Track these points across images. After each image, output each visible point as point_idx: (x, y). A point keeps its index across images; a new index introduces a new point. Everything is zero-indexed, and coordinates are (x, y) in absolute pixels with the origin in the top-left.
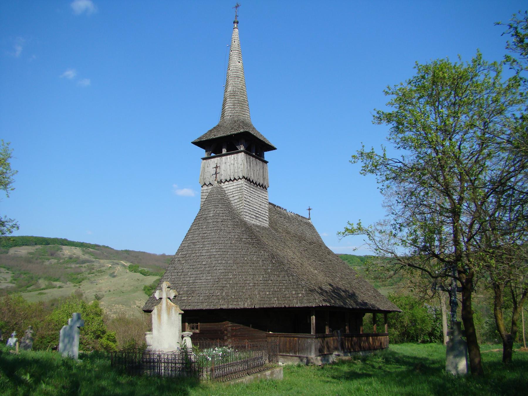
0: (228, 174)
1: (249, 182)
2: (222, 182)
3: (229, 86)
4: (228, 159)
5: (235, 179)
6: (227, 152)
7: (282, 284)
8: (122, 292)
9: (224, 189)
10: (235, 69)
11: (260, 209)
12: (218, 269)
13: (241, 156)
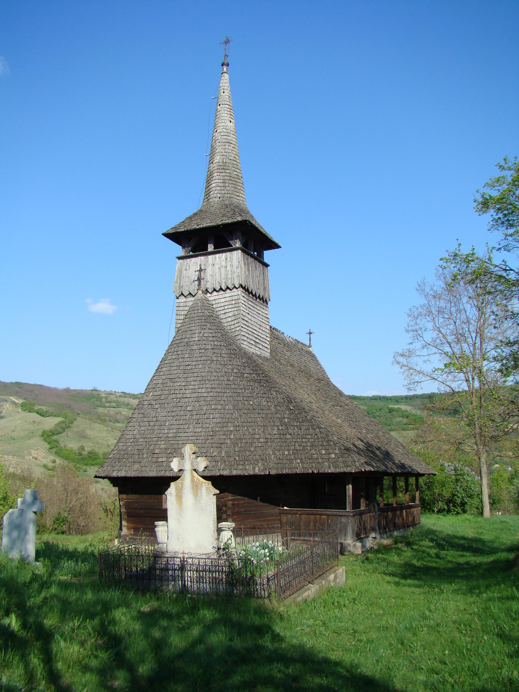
0: (217, 281)
1: (247, 293)
3: (216, 155)
4: (217, 259)
5: (228, 288)
6: (214, 249)
7: (306, 440)
8: (12, 439)
9: (212, 302)
10: (225, 130)
11: (260, 331)
12: (211, 417)
13: (237, 255)
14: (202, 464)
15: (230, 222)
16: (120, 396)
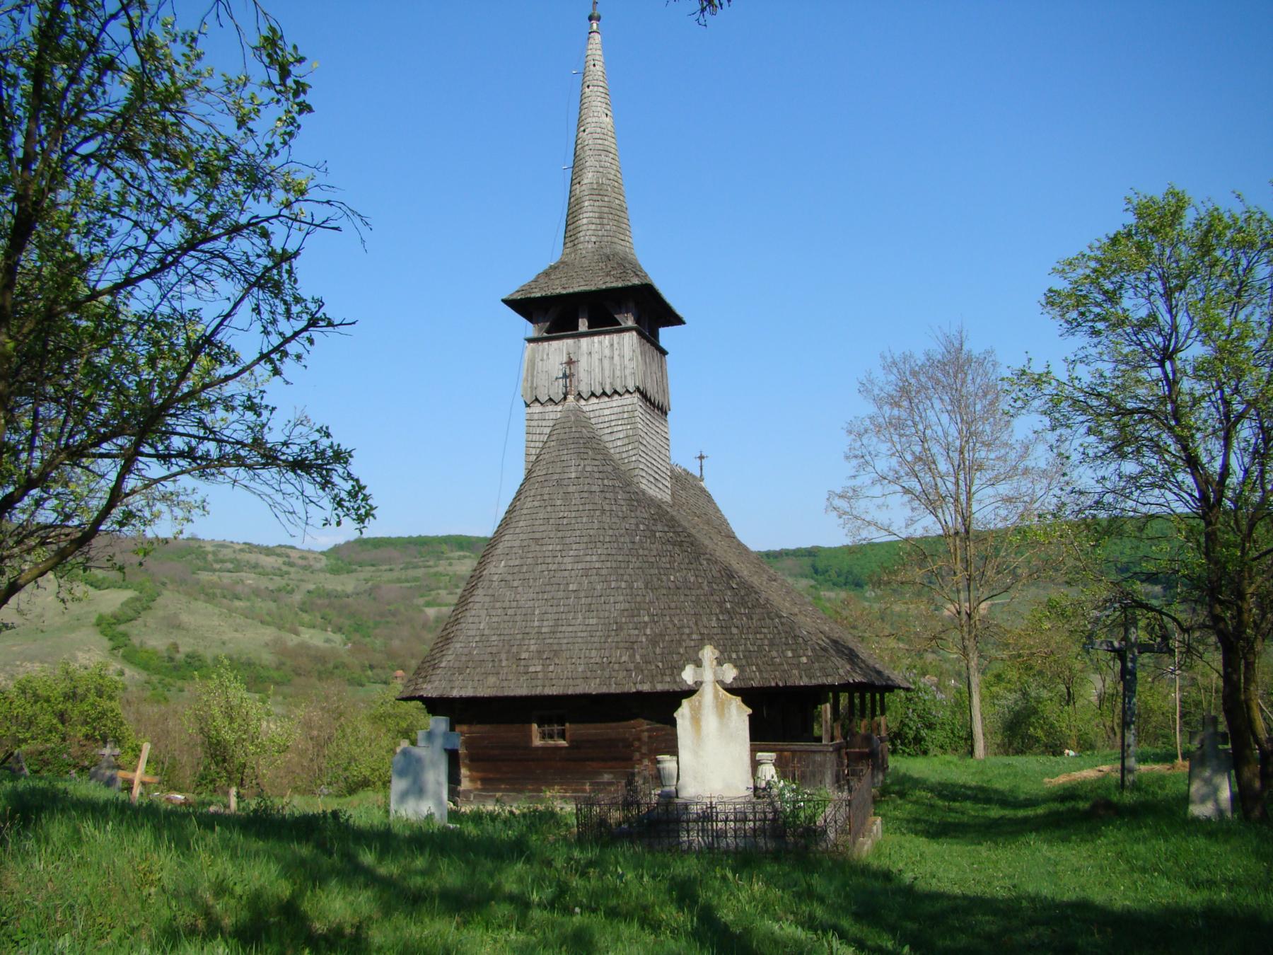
2: (582, 397)
3: (585, 171)
4: (596, 345)
5: (616, 392)
6: (590, 327)
7: (762, 636)
10: (599, 130)
14: (730, 673)
15: (620, 285)
16: (242, 550)
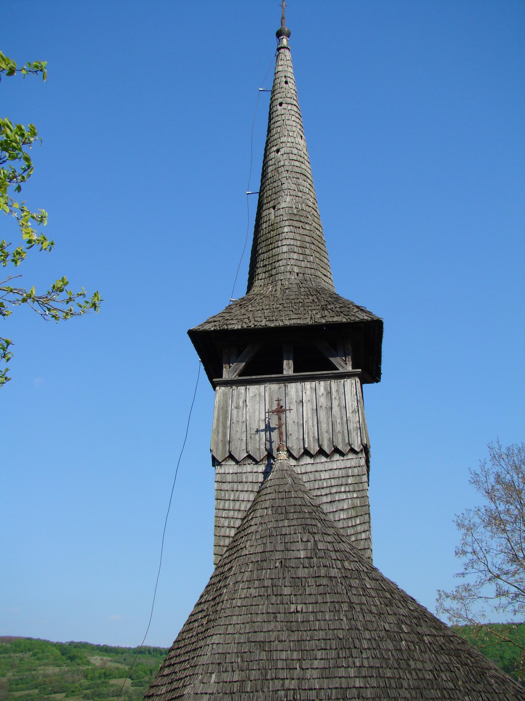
5: (337, 451)
